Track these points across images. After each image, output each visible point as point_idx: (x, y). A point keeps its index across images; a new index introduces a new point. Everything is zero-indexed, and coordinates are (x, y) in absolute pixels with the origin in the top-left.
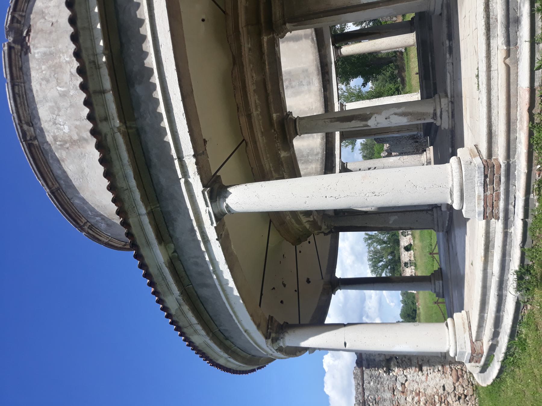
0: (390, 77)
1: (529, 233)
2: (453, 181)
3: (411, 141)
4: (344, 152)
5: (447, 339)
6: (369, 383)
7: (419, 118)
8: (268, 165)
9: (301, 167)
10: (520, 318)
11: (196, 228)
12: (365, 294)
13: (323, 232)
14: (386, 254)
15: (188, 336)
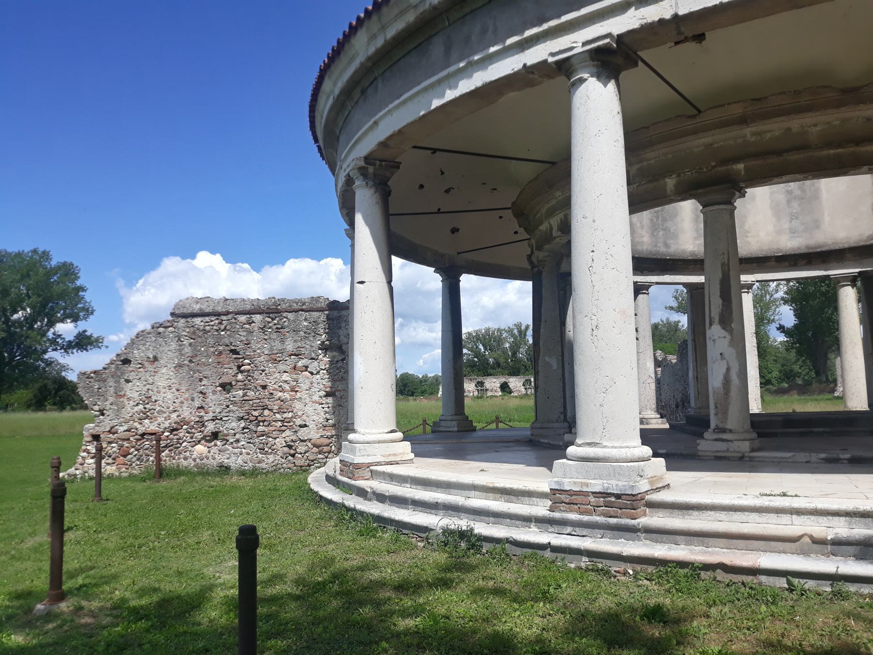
0: (792, 371)
1: (529, 551)
2: (613, 447)
3: (679, 397)
4: (667, 290)
5: (374, 431)
6: (306, 320)
7: (719, 406)
8: (653, 156)
9: (646, 216)
10: (405, 531)
11: (545, 26)
12: (436, 322)
13: (532, 252)
14: (495, 355)
15: (366, 24)
